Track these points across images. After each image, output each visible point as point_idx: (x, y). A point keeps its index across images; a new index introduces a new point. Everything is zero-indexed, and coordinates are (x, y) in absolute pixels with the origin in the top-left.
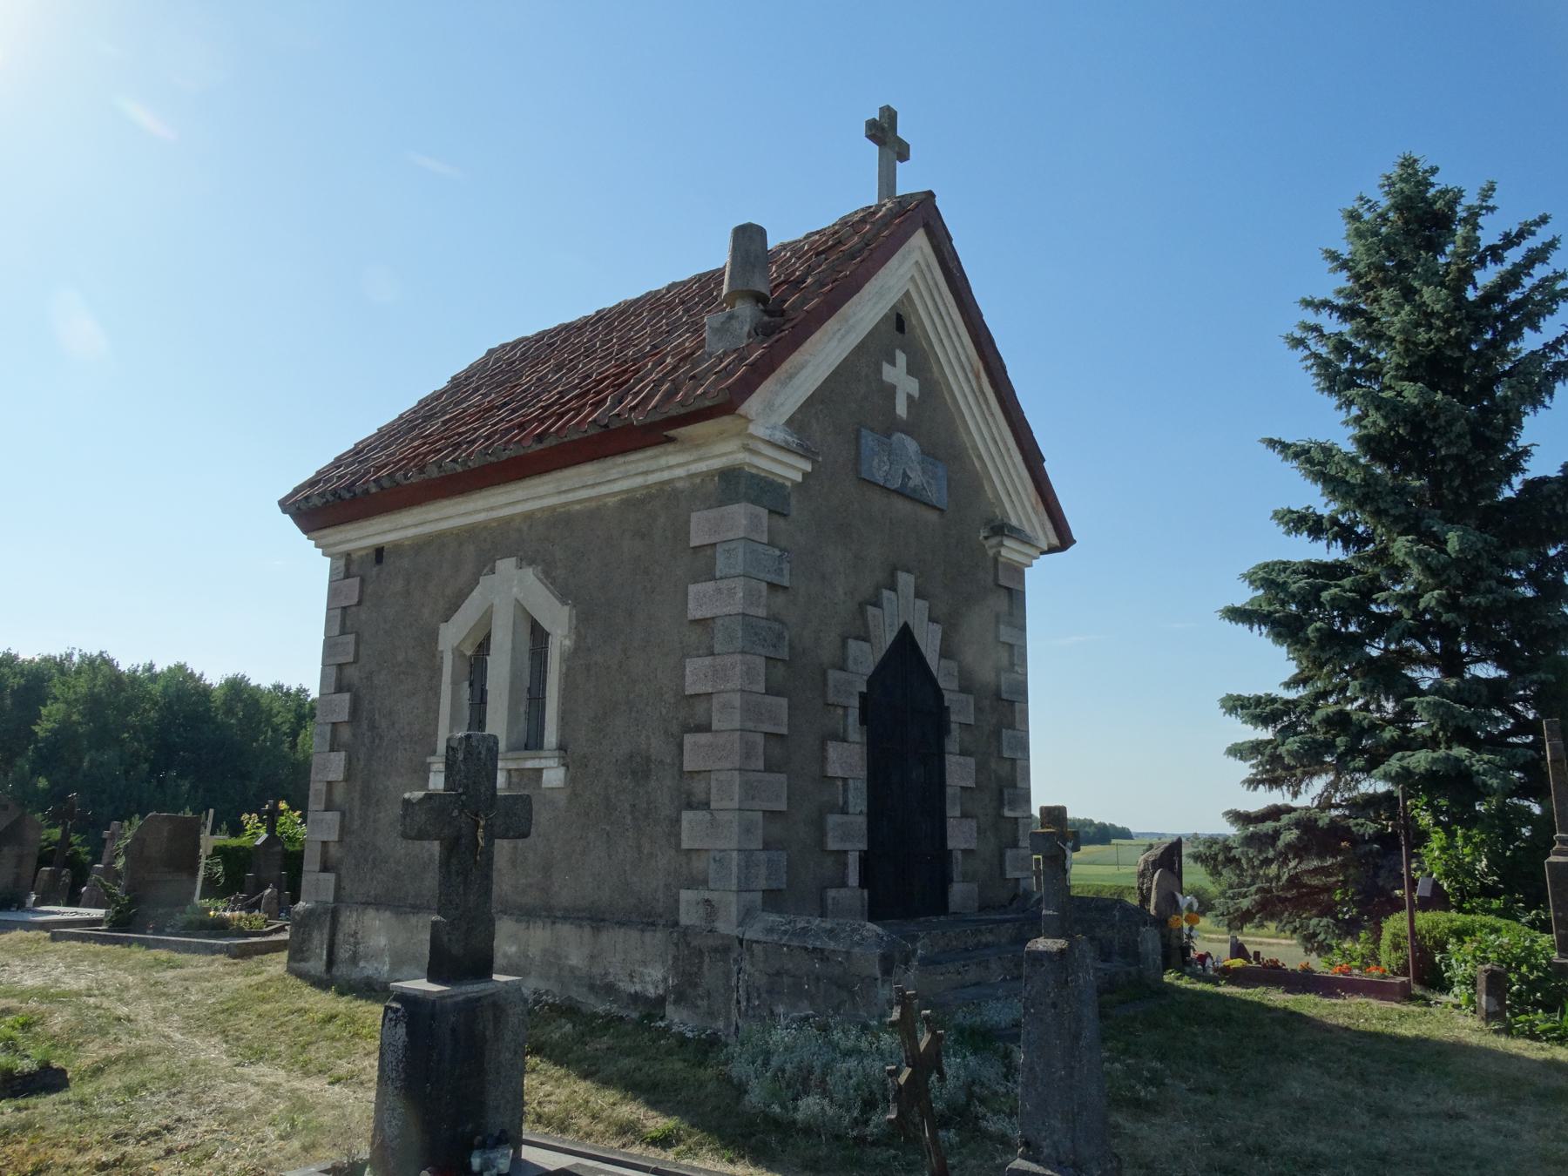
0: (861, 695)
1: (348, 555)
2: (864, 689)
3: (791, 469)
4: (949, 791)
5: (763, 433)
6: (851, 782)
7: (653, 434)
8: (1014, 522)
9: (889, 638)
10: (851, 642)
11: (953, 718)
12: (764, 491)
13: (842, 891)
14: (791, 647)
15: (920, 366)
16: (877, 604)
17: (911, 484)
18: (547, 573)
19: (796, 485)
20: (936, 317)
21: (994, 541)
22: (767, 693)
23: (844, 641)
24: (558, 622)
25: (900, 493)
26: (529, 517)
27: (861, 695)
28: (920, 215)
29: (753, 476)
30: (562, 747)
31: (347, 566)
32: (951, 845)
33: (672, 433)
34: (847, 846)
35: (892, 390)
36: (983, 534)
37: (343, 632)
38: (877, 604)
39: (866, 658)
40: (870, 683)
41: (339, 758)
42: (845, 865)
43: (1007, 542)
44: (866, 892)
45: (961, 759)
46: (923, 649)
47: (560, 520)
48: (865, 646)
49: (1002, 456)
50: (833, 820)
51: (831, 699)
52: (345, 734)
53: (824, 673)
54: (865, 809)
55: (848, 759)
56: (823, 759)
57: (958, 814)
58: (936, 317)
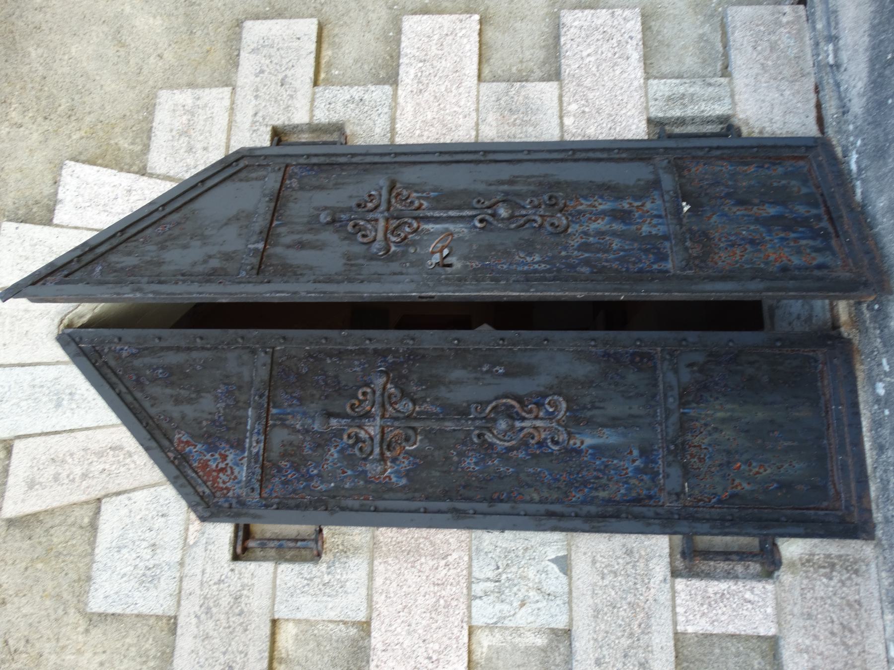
0: (242, 551)
2: (223, 533)
4: (492, 131)
9: (89, 409)
11: (300, 117)
32: (634, 128)
44: (792, 549)
45: (407, 73)
57: (550, 89)
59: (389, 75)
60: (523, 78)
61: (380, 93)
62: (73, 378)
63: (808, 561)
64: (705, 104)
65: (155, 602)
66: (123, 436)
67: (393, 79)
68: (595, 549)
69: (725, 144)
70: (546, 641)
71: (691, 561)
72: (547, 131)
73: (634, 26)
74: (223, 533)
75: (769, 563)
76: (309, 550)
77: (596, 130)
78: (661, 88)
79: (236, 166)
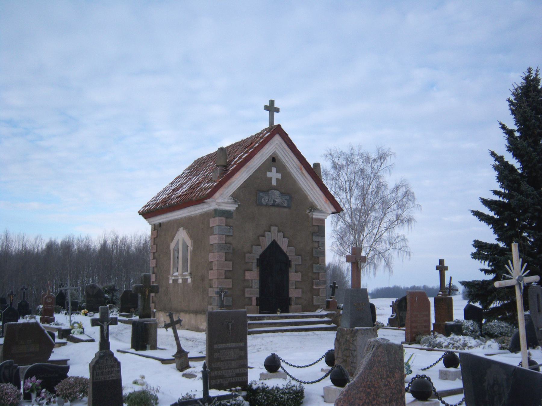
0: (257, 259)
1: (155, 225)
2: (259, 258)
3: (232, 207)
4: (290, 282)
5: (223, 200)
6: (254, 281)
7: (200, 201)
8: (319, 207)
9: (268, 244)
10: (253, 246)
11: (292, 263)
12: (226, 214)
13: (251, 307)
14: (233, 249)
15: (282, 169)
16: (264, 236)
17: (276, 203)
18: (188, 231)
19: (235, 210)
20: (285, 157)
21: (311, 213)
22: (226, 261)
23: (252, 246)
24: (189, 242)
25: (273, 205)
26: (185, 217)
27: (257, 259)
28: (276, 131)
29: (220, 210)
30: (191, 273)
31: (155, 227)
32: (290, 296)
33: (205, 201)
34: (252, 296)
35: (270, 179)
36: (308, 211)
37: (154, 244)
38: (264, 236)
39: (259, 251)
40: (260, 256)
41: (154, 275)
42: (252, 301)
43: (314, 213)
44: (258, 307)
45: (296, 274)
46: (281, 245)
47: (190, 219)
48: (259, 247)
49: (312, 190)
50: (246, 290)
51: (247, 261)
52: (155, 270)
53: (245, 255)
54: (258, 287)
55: (253, 276)
56: (244, 276)
57: (294, 288)
58: (285, 157)
59: (296, 272)
60: (295, 285)
61: (294, 270)
62: (270, 242)
63: (83, 384)
64: (293, 303)
65: (254, 252)
66: (266, 248)
67: (296, 272)
68: (258, 290)
69: (204, 373)
70: (133, 293)
71: (257, 298)
72: (290, 287)
73: (300, 296)
74: (259, 258)
75: (257, 305)
76: (257, 266)
77: (290, 292)
78: (294, 299)
79: (287, 257)
